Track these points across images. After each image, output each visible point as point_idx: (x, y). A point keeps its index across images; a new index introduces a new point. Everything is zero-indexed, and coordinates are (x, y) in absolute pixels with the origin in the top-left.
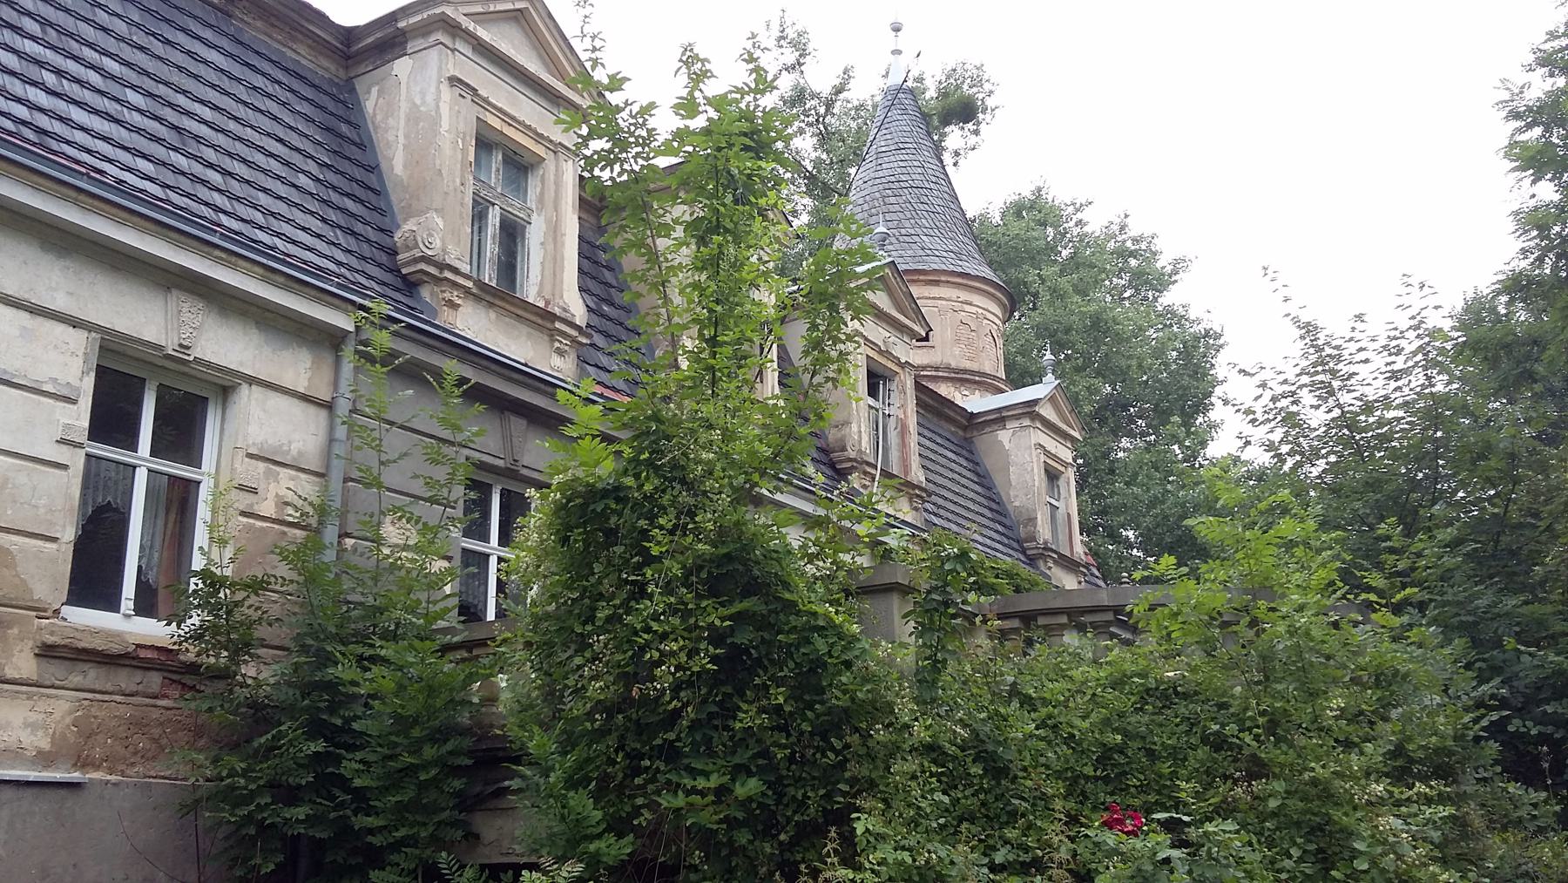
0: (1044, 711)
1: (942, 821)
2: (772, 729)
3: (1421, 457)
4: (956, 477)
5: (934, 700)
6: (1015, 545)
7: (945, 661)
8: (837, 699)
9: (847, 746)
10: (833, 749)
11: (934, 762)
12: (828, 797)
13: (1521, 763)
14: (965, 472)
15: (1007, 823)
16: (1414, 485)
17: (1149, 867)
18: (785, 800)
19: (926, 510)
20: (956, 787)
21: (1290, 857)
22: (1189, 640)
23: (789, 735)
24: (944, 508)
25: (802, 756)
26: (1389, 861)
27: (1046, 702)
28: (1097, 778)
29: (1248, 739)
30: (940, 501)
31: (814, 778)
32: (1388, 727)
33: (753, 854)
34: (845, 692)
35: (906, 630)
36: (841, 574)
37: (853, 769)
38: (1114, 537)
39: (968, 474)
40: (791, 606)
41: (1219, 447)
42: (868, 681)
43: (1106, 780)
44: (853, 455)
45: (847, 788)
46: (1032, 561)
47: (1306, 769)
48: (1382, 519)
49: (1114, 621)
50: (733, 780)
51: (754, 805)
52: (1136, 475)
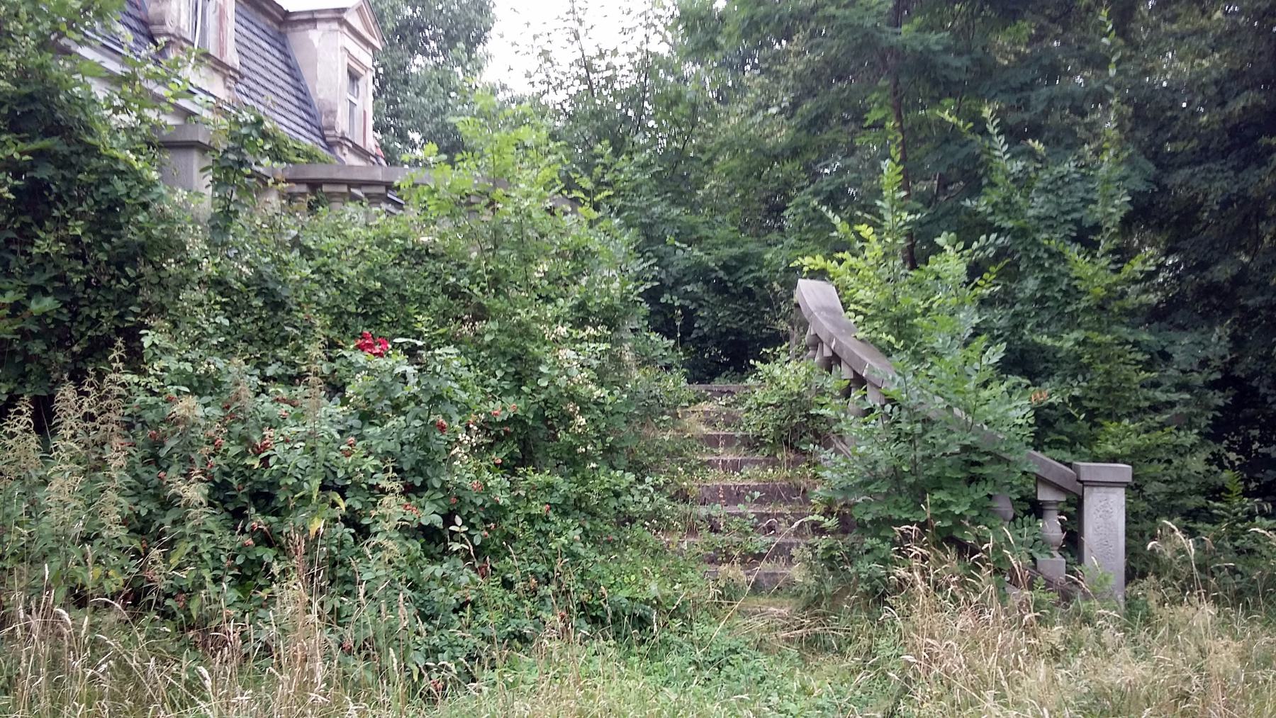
0: (320, 260)
1: (222, 339)
2: (70, 256)
3: (634, 97)
4: (269, 65)
5: (224, 244)
6: (317, 132)
7: (236, 212)
8: (132, 235)
9: (141, 275)
10: (127, 277)
11: (222, 294)
12: (121, 317)
13: (662, 322)
14: (276, 62)
15: (280, 346)
16: (626, 118)
17: (388, 380)
18: (80, 318)
19: (238, 91)
20: (238, 315)
21: (495, 376)
22: (442, 212)
23: (85, 263)
24: (255, 91)
25: (98, 282)
26: (562, 381)
27: (322, 253)
28: (358, 315)
29: (476, 290)
30: (252, 85)
31: (108, 301)
32: (576, 288)
33: (46, 362)
34: (141, 229)
35: (203, 183)
36: (145, 128)
37: (145, 295)
38: (402, 137)
39: (280, 65)
40: (92, 150)
41: (490, 75)
42: (163, 222)
43: (365, 316)
44: (171, 30)
45: (137, 310)
46: (330, 146)
47: (515, 314)
48: (599, 141)
49: (383, 193)
50: (29, 298)
51: (49, 321)
52: (425, 87)
